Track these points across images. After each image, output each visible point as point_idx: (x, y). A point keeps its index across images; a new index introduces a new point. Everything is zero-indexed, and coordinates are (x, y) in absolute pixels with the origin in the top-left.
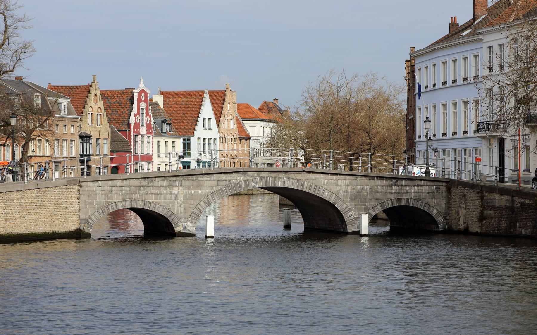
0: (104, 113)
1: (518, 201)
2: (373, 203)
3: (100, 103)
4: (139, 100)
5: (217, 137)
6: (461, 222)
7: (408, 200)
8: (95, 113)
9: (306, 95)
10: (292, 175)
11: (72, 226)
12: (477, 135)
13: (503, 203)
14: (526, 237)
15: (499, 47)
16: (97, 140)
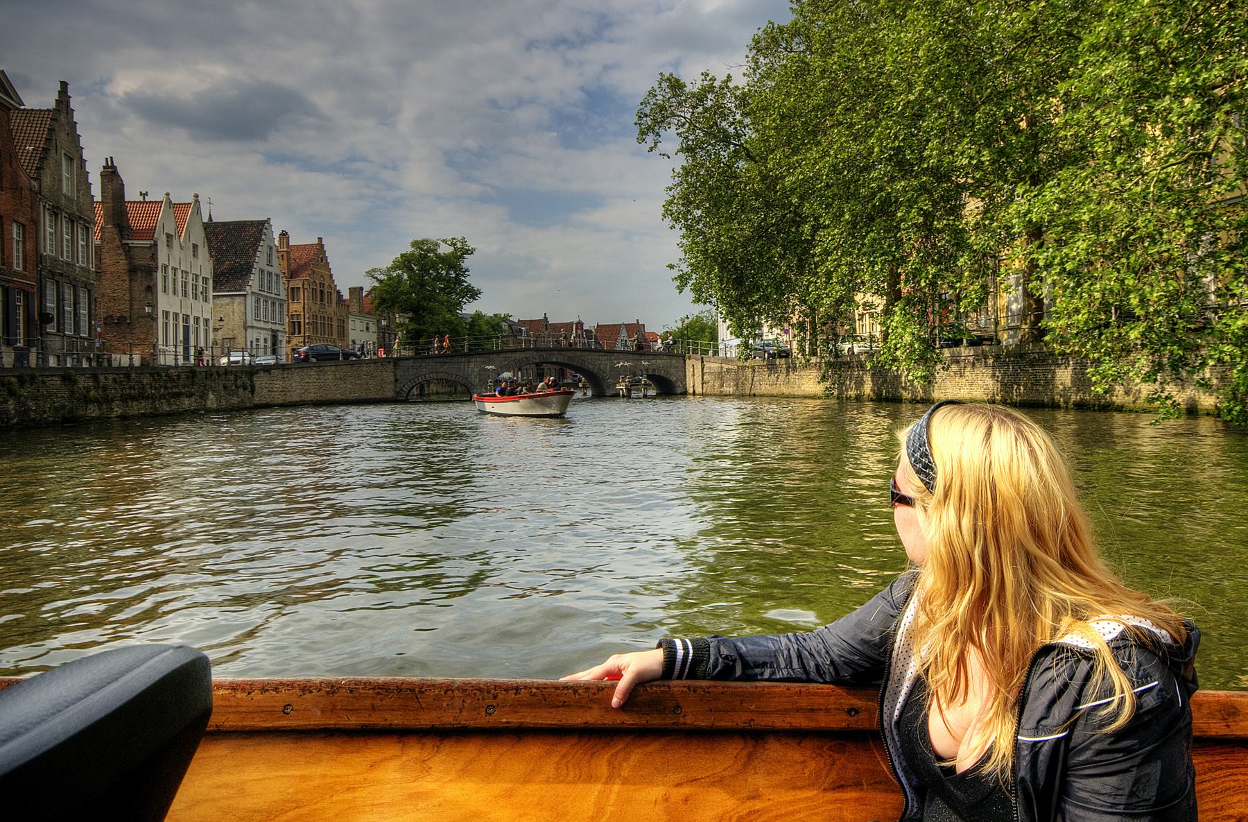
4: (577, 329)
7: (654, 370)
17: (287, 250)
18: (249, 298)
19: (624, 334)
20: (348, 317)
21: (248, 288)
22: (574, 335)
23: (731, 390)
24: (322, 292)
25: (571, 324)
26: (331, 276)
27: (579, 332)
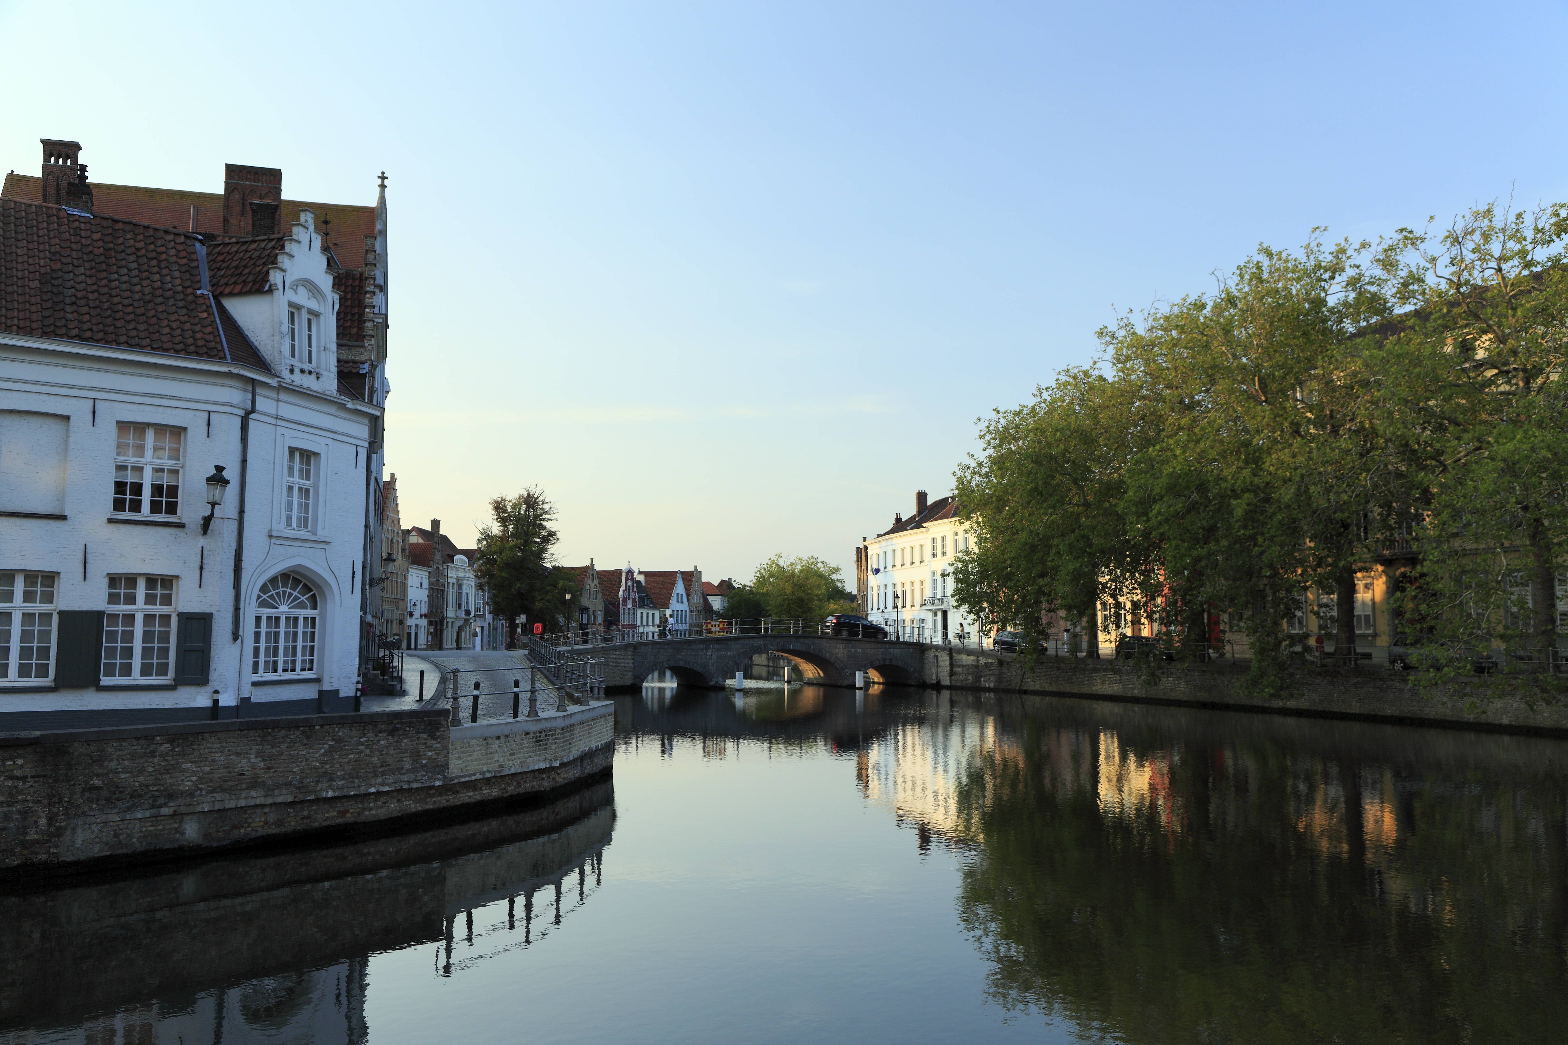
0: (598, 589)
1: (982, 660)
3: (596, 582)
4: (627, 579)
5: (687, 609)
6: (934, 677)
7: (891, 660)
8: (592, 589)
9: (758, 575)
10: (801, 640)
12: (923, 608)
13: (970, 663)
15: (210, 506)
16: (594, 612)
23: (992, 685)
25: (619, 572)
27: (630, 583)
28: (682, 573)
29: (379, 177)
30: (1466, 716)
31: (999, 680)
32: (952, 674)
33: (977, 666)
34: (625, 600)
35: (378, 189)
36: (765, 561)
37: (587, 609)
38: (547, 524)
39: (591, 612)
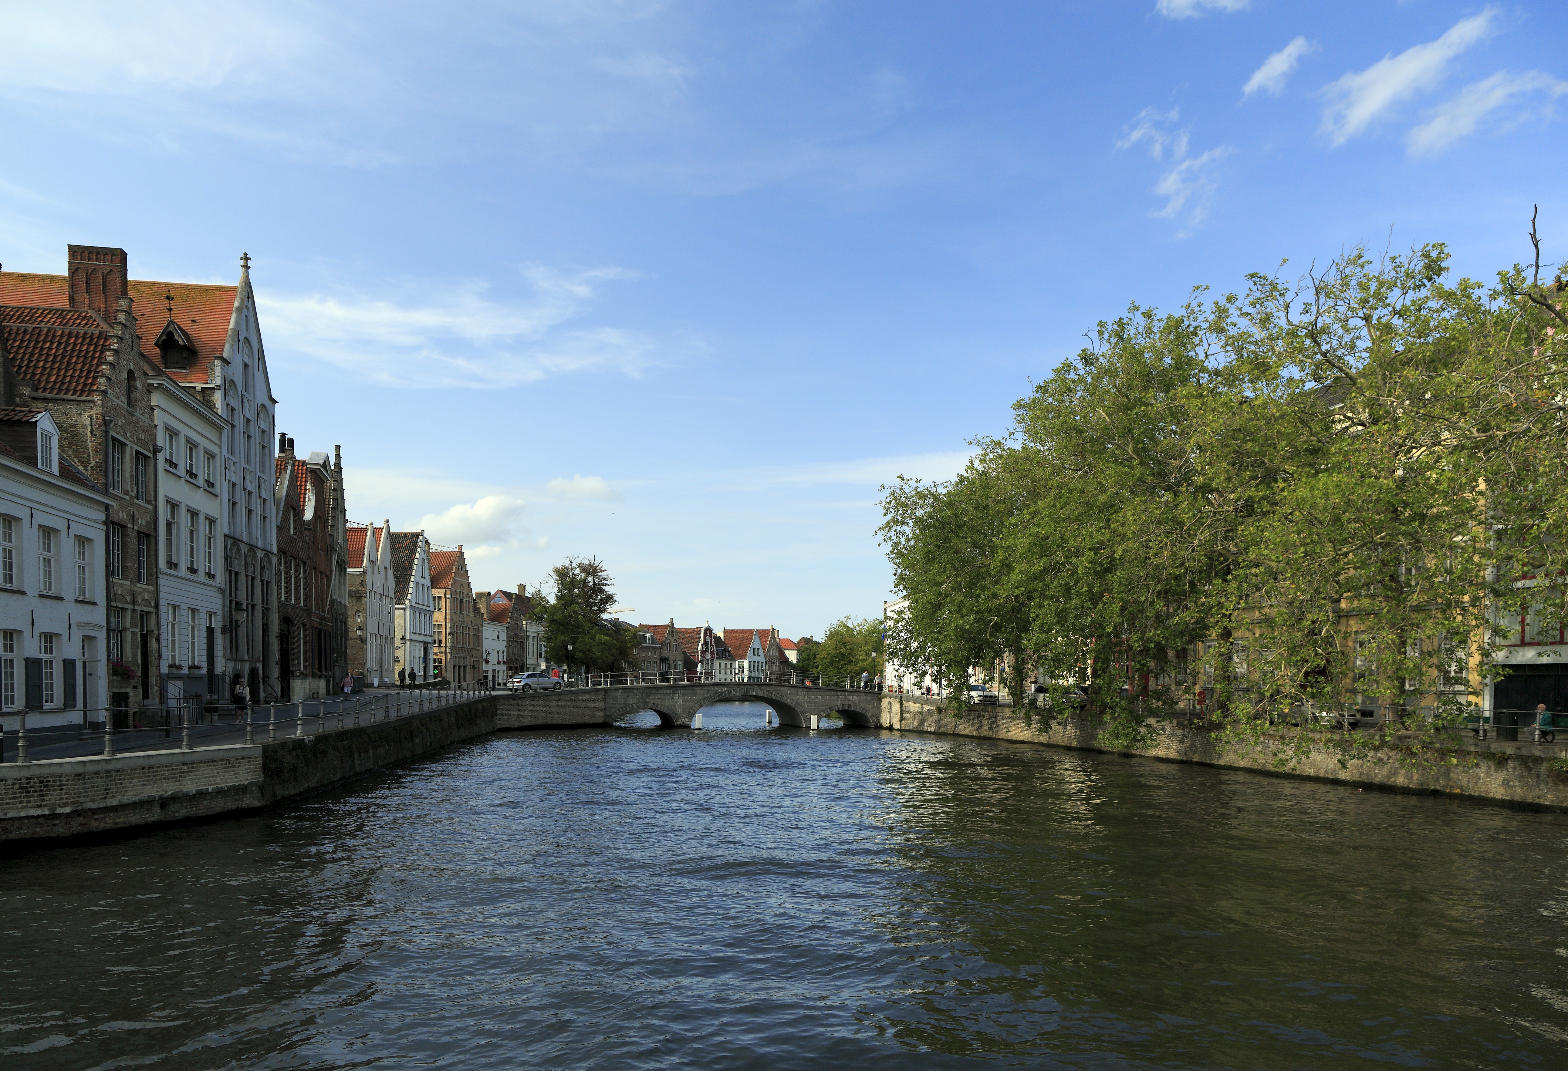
2: (824, 708)
4: (705, 635)
7: (850, 706)
8: (672, 643)
10: (764, 688)
11: (599, 718)
13: (916, 709)
14: (930, 733)
17: (432, 557)
18: (408, 612)
19: (756, 643)
20: (482, 626)
21: (407, 601)
22: (702, 641)
23: (933, 730)
24: (461, 600)
25: (698, 630)
26: (469, 584)
27: (708, 639)
28: (759, 631)
29: (241, 258)
30: (1307, 769)
31: (938, 725)
32: (902, 719)
33: (921, 713)
34: (703, 653)
35: (242, 270)
36: (835, 623)
37: (668, 659)
38: (606, 588)
39: (671, 662)
